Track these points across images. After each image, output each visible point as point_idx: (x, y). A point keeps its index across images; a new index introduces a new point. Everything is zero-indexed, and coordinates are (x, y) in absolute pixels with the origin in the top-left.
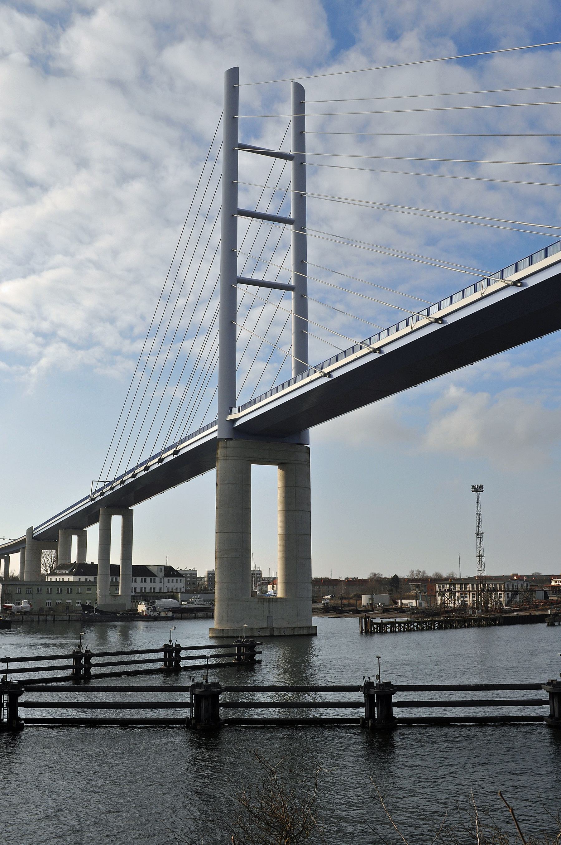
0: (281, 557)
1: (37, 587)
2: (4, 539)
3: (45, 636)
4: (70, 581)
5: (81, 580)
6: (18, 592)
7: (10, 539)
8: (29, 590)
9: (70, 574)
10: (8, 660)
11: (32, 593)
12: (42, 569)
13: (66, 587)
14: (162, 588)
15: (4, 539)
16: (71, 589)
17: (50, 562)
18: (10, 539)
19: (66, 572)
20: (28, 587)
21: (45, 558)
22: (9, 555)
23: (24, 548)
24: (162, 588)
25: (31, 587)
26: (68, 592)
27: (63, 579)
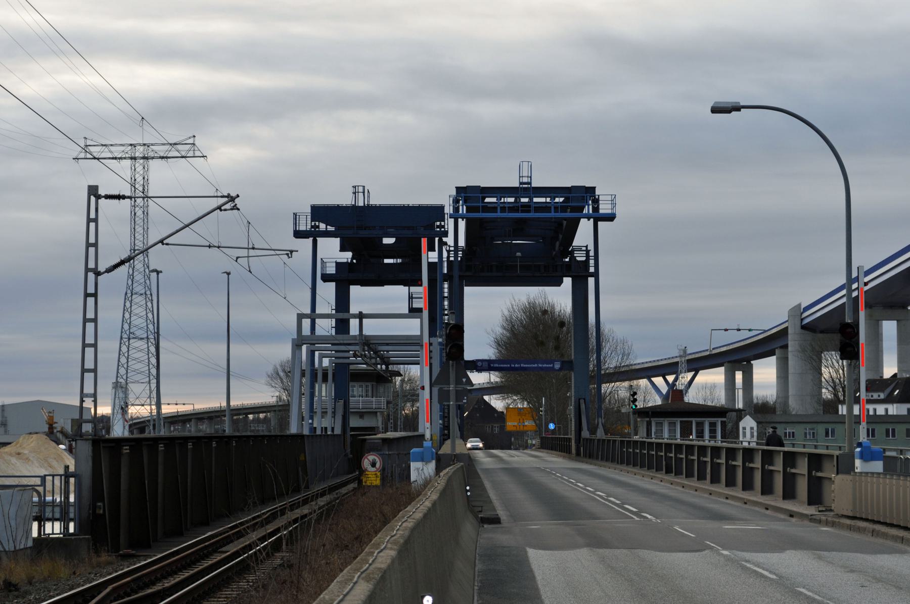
0: (553, 307)
1: (827, 426)
2: (739, 330)
3: (621, 525)
4: (877, 414)
5: (890, 413)
6: (789, 437)
7: (750, 330)
8: (810, 433)
9: (889, 400)
10: (902, 540)
11: (815, 438)
12: (614, 384)
13: (885, 427)
14: (425, 422)
15: (739, 330)
16: (893, 430)
17: (842, 376)
18: (750, 330)
19: (879, 396)
20: (809, 426)
21: (830, 368)
22: (752, 362)
23: (786, 347)
24: (425, 422)
25: (814, 426)
26: (888, 435)
27: (875, 410)
